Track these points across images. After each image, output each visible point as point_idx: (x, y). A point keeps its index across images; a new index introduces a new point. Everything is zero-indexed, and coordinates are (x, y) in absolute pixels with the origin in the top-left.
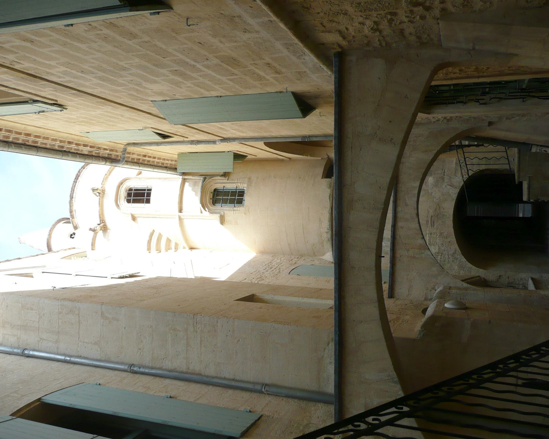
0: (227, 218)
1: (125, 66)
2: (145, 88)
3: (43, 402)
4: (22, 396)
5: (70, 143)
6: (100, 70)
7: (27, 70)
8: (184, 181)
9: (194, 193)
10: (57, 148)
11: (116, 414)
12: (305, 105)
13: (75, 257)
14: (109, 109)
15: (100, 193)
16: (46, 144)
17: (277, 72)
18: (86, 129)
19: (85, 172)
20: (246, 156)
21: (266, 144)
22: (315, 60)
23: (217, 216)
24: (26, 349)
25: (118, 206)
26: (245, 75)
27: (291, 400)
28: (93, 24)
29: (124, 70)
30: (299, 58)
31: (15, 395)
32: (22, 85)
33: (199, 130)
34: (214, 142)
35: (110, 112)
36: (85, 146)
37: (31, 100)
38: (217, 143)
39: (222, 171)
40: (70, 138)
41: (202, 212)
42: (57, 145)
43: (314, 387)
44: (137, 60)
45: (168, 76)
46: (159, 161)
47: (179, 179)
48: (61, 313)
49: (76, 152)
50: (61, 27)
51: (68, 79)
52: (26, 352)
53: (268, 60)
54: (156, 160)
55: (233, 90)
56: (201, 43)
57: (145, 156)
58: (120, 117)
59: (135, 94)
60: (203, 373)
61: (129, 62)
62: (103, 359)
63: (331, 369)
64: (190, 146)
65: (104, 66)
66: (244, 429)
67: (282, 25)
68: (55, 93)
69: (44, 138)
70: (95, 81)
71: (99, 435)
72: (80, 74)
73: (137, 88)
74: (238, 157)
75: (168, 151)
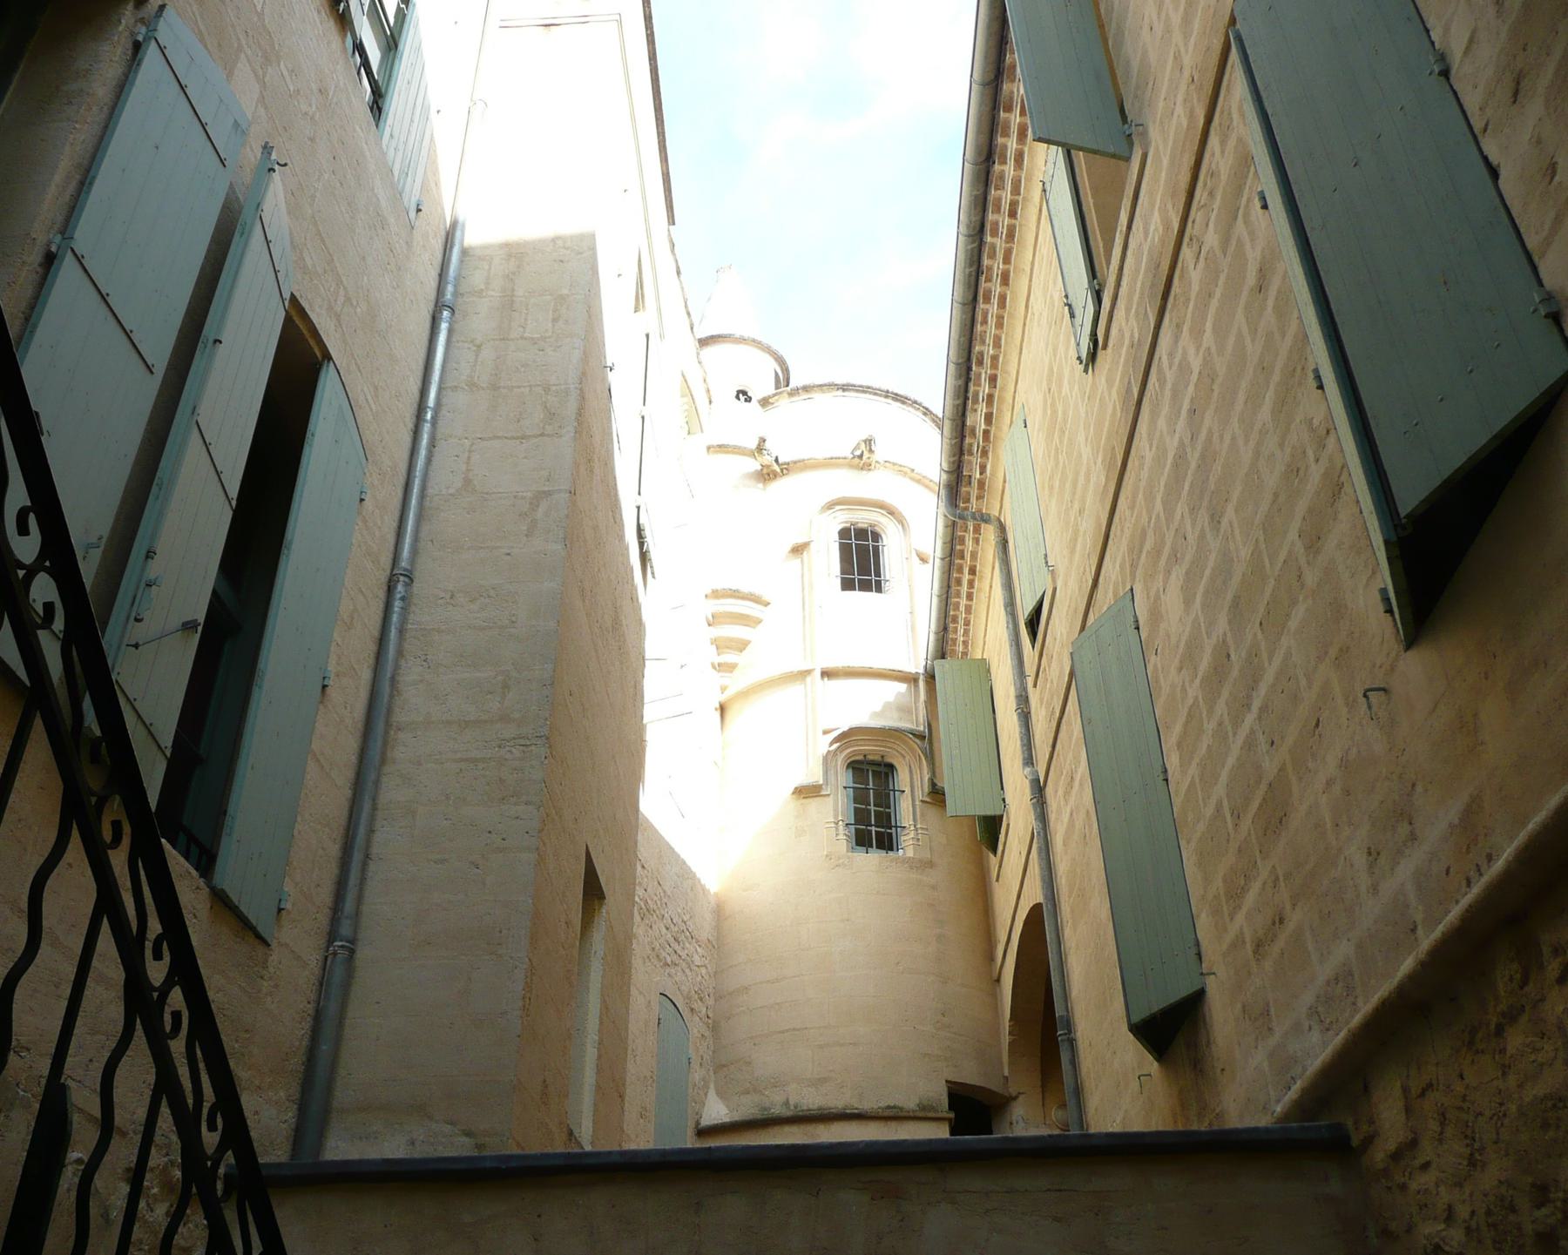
0: (813, 805)
1: (1225, 522)
2: (1168, 572)
3: (321, 366)
4: (338, 317)
5: (993, 379)
6: (1203, 457)
7: (1182, 277)
8: (911, 679)
9: (878, 708)
11: (284, 551)
12: (1170, 1030)
14: (1098, 478)
15: (862, 459)
16: (985, 322)
17: (1259, 946)
18: (1035, 420)
19: (915, 417)
20: (995, 851)
21: (1036, 911)
22: (1316, 1063)
23: (815, 775)
24: (453, 311)
25: (831, 506)
26: (1240, 851)
27: (307, 1025)
28: (1331, 440)
29: (1212, 517)
30: (1313, 1012)
31: (341, 299)
32: (1138, 262)
33: (1061, 718)
34: (1029, 760)
35: (1088, 479)
36: (989, 418)
38: (1028, 770)
39: (945, 784)
41: (825, 732)
43: (343, 1095)
44: (1245, 553)
45: (1209, 635)
46: (962, 608)
47: (916, 665)
48: (547, 389)
49: (970, 395)
50: (1310, 359)
51: (1170, 376)
52: (446, 314)
53: (1294, 918)
54: (963, 602)
55: (1190, 817)
56: (1317, 725)
57: (973, 571)
58: (1076, 506)
59: (1148, 546)
60: (387, 769)
61: (1237, 532)
62: (427, 504)
63: (392, 1147)
65: (1217, 468)
66: (234, 898)
67: (1407, 965)
68: (1127, 342)
69: (1000, 318)
70: (1172, 445)
71: (235, 512)
72: (1186, 406)
74: (991, 829)
75: (991, 635)
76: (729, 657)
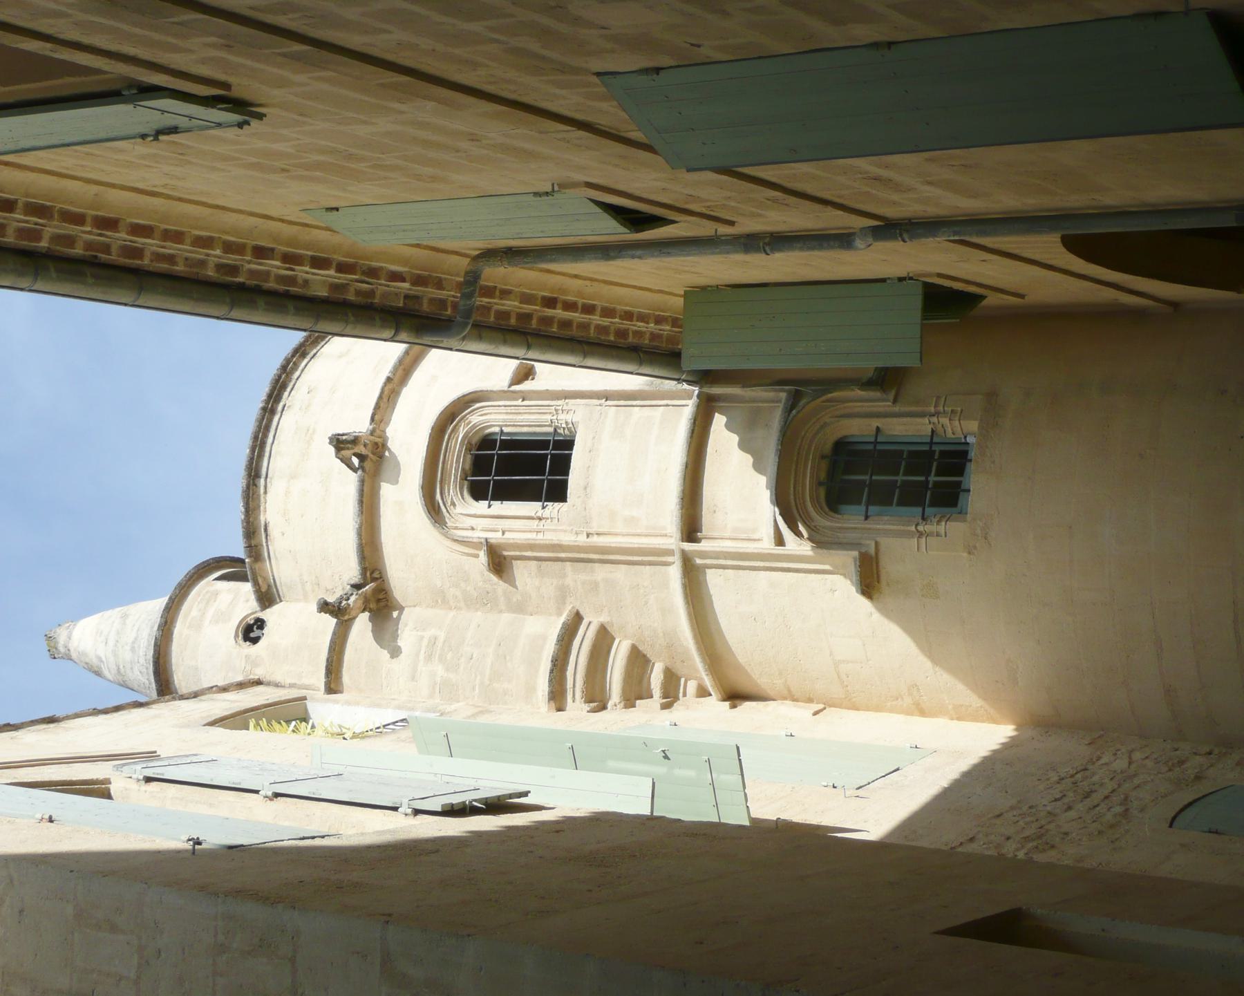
0: (891, 567)
5: (261, 252)
9: (748, 459)
10: (211, 273)
13: (264, 723)
14: (426, 111)
15: (365, 455)
16: (171, 259)
18: (327, 194)
20: (983, 297)
21: (1074, 244)
23: (848, 558)
34: (843, 240)
36: (319, 263)
37: (130, 87)
38: (859, 243)
39: (868, 365)
40: (263, 233)
41: (780, 541)
42: (212, 261)
49: (281, 288)
57: (550, 302)
58: (465, 145)
59: (534, 46)
64: (739, 257)
68: (222, 54)
73: (546, 21)
74: (944, 302)
75: (648, 282)
76: (656, 679)
